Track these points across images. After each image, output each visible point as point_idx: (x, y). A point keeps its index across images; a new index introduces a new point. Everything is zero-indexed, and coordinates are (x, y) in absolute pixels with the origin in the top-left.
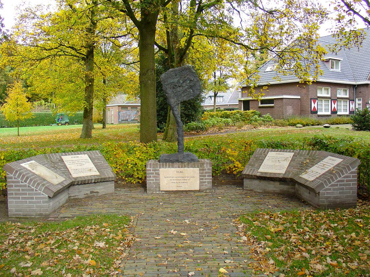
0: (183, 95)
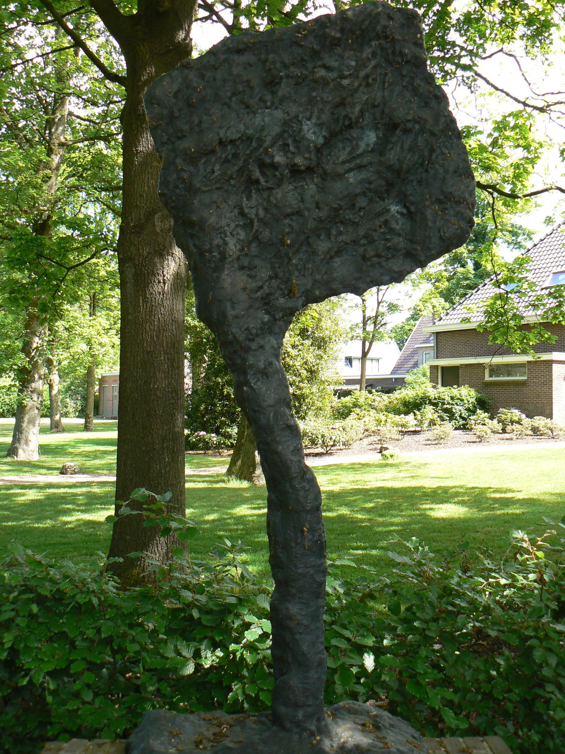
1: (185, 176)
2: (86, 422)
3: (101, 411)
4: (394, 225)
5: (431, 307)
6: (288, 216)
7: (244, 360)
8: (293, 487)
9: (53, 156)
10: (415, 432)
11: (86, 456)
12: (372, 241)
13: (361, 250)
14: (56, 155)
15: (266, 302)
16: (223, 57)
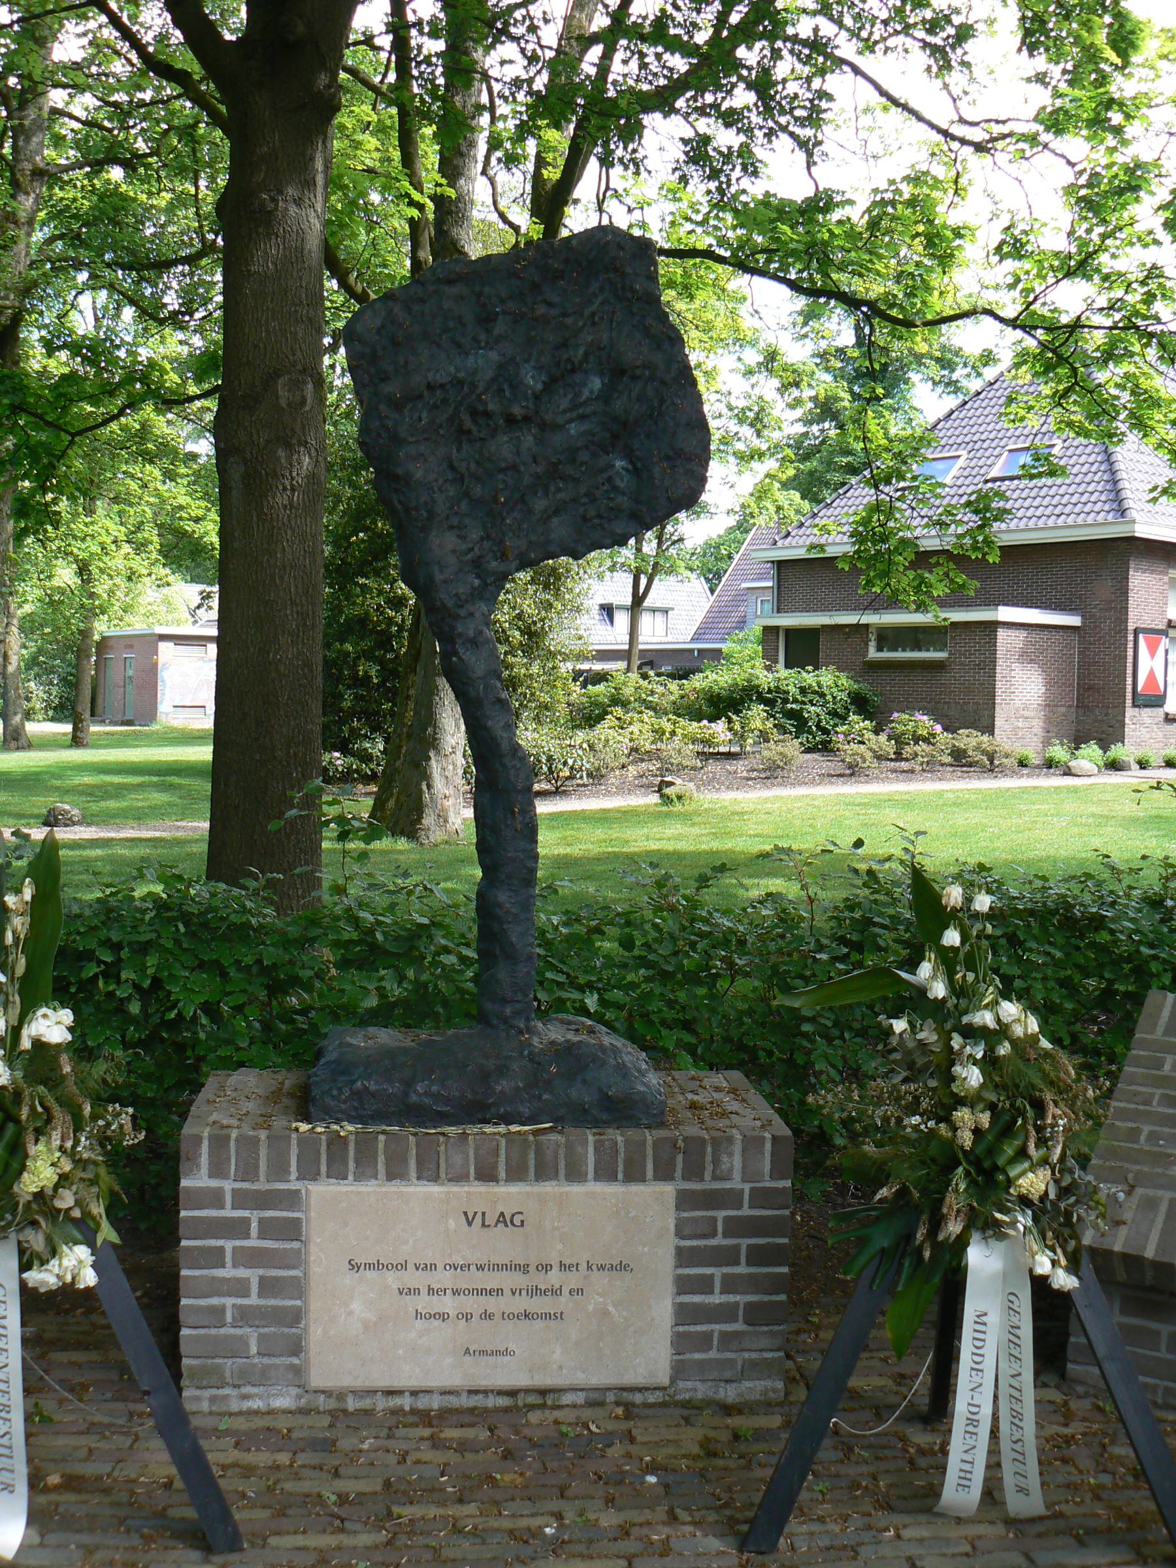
0: (540, 504)
1: (390, 424)
2: (75, 729)
3: (99, 709)
4: (618, 482)
5: (772, 509)
6: (501, 470)
7: (453, 628)
8: (503, 765)
9: (21, 198)
10: (729, 756)
11: (90, 795)
12: (593, 500)
13: (581, 510)
14: (27, 194)
15: (477, 565)
16: (431, 288)
